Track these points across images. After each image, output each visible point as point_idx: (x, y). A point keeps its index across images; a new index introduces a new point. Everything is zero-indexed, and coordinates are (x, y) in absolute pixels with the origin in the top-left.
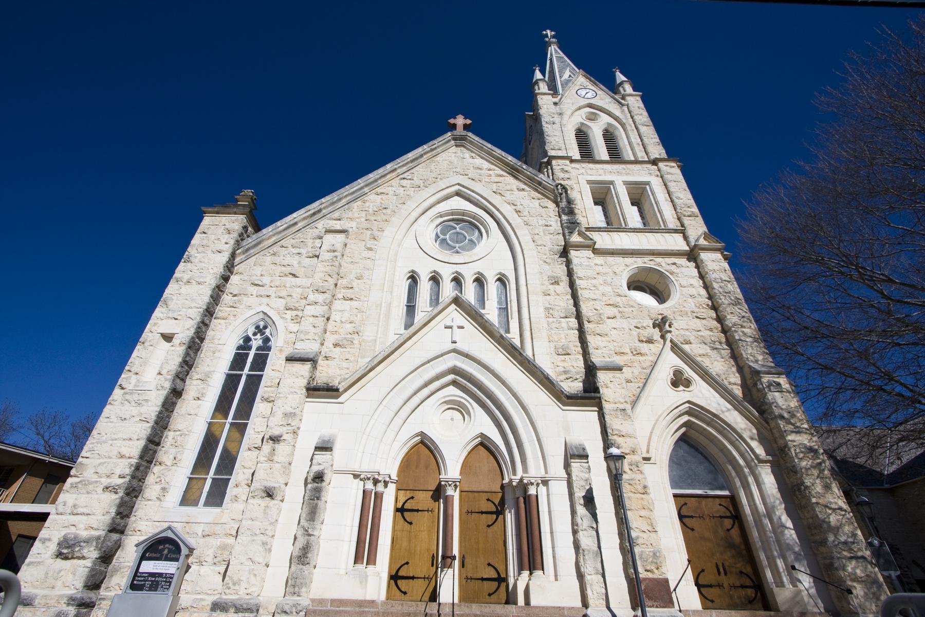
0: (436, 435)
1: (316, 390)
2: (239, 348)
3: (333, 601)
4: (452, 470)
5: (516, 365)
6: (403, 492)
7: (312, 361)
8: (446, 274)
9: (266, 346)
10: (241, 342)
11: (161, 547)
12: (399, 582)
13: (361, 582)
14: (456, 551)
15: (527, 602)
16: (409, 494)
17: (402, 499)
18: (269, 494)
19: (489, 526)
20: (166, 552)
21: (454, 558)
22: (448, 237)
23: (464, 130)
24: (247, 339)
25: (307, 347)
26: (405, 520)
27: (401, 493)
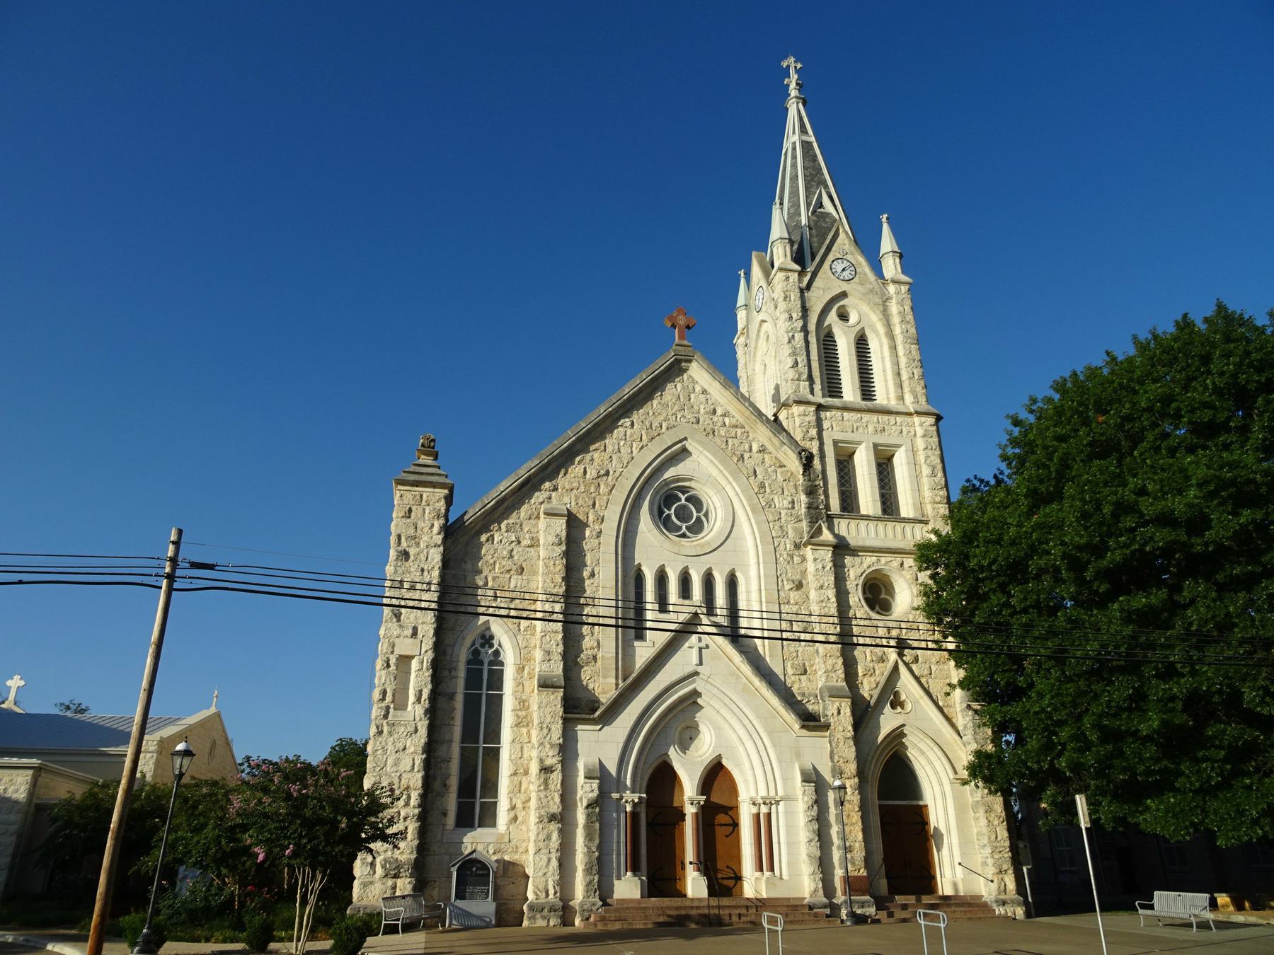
10: (471, 657)
19: (727, 836)
22: (672, 511)
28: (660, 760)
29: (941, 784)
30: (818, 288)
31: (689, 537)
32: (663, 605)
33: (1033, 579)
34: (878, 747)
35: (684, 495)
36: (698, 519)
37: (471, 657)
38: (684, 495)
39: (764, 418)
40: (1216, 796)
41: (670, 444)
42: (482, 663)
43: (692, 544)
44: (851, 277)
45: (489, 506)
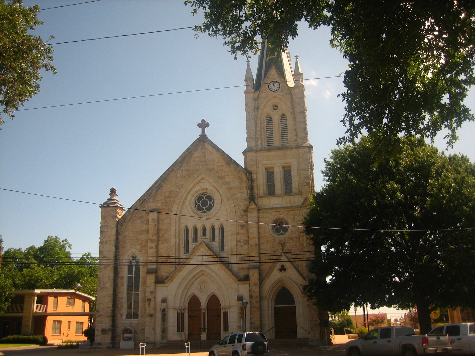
0: (198, 294)
14: (206, 327)
28: (193, 295)
31: (206, 212)
36: (210, 204)
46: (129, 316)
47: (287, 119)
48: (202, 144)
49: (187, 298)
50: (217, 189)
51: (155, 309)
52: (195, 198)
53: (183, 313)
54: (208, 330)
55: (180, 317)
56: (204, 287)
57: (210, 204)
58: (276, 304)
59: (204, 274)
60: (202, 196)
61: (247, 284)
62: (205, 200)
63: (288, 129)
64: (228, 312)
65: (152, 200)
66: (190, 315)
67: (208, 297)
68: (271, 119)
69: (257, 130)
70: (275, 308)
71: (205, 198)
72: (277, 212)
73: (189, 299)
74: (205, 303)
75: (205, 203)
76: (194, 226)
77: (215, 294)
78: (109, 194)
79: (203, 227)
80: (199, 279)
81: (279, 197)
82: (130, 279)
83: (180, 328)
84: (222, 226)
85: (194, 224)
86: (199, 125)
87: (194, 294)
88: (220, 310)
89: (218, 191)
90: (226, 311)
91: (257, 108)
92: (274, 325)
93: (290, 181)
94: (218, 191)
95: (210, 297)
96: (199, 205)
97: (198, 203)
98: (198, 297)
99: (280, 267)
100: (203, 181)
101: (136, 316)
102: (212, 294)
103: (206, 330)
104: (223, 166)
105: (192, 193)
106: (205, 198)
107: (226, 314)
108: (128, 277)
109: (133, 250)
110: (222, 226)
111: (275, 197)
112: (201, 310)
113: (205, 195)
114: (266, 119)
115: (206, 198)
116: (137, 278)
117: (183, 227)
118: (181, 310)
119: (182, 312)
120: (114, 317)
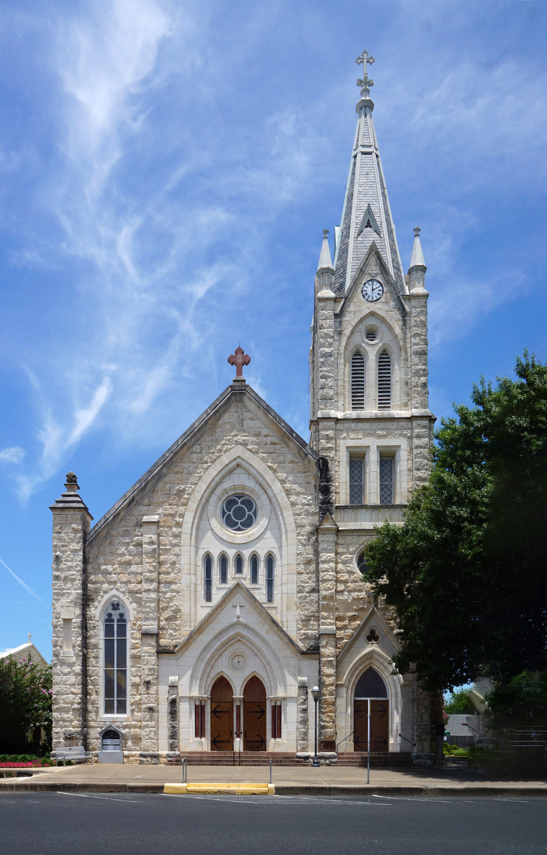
0: (229, 674)
1: (162, 652)
2: (106, 621)
3: (189, 753)
4: (238, 693)
5: (178, 794)
6: (214, 703)
7: (157, 636)
8: (231, 553)
9: (122, 619)
10: (107, 617)
11: (109, 733)
12: (216, 743)
13: (200, 745)
14: (242, 730)
15: (183, 767)
16: (217, 704)
17: (214, 706)
18: (151, 709)
19: (258, 718)
20: (112, 735)
21: (241, 733)
22: (231, 513)
23: (196, 736)
24: (110, 615)
25: (152, 626)
26: (217, 717)
27: (214, 704)
28: (219, 675)
29: (396, 688)
30: (350, 312)
31: (243, 530)
32: (224, 579)
33: (121, 564)
34: (281, 668)
35: (239, 499)
36: (249, 516)
37: (107, 617)
38: (239, 499)
39: (294, 435)
40: (93, 719)
41: (227, 462)
42: (113, 621)
43: (240, 537)
44: (378, 297)
45: (109, 520)
46: (109, 709)
47: (389, 362)
48: (238, 397)
49: (210, 679)
50: (263, 488)
51: (157, 700)
52: (223, 502)
53: (204, 706)
54: (245, 736)
55: (199, 711)
56: (239, 662)
57: (249, 516)
58: (356, 696)
59: (239, 640)
60: (235, 500)
61: (315, 659)
62: (239, 507)
63: (351, 394)
64: (281, 706)
65: (146, 501)
66: (213, 709)
67: (246, 679)
68: (362, 359)
69: (339, 378)
70: (355, 701)
71: (239, 504)
72: (367, 536)
73: (214, 682)
74: (241, 690)
75: (239, 513)
76: (221, 555)
77: (257, 676)
78: (65, 485)
79: (252, 557)
80: (231, 649)
81: (372, 510)
82: (109, 644)
83: (200, 732)
84: (239, 557)
85: (206, 550)
86: (232, 361)
87: (222, 674)
88: (265, 702)
89: (266, 492)
90: (278, 704)
91: (339, 334)
92: (353, 730)
93: (389, 482)
94: (266, 492)
95: (248, 679)
96: (229, 516)
97: (228, 513)
98: (228, 679)
99: (369, 633)
100: (239, 470)
101: (122, 708)
102: (252, 676)
103: (242, 735)
104: (275, 444)
105: (218, 491)
106: (239, 504)
107: (277, 711)
108: (106, 640)
109: (114, 592)
110: (269, 556)
111: (365, 510)
112: (232, 702)
113: (239, 497)
114: (353, 359)
115: (242, 503)
116: (122, 644)
117: (202, 553)
118: (201, 701)
119: (203, 704)
120: (84, 712)
